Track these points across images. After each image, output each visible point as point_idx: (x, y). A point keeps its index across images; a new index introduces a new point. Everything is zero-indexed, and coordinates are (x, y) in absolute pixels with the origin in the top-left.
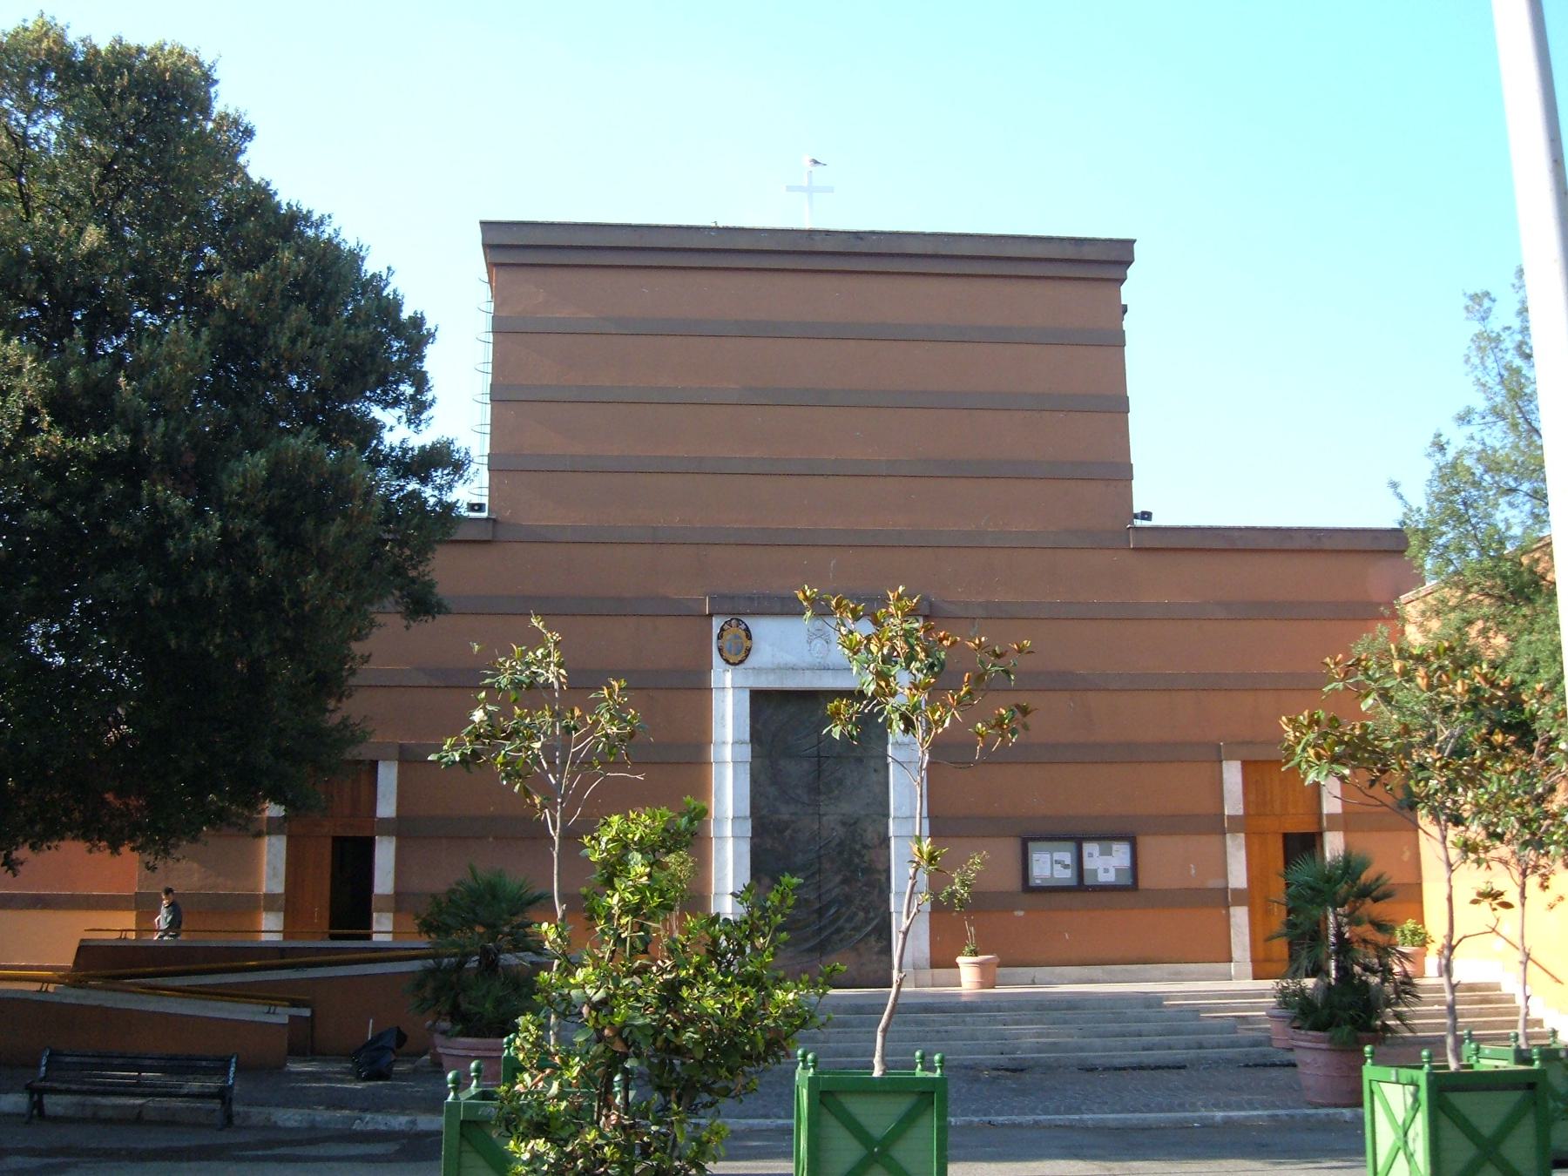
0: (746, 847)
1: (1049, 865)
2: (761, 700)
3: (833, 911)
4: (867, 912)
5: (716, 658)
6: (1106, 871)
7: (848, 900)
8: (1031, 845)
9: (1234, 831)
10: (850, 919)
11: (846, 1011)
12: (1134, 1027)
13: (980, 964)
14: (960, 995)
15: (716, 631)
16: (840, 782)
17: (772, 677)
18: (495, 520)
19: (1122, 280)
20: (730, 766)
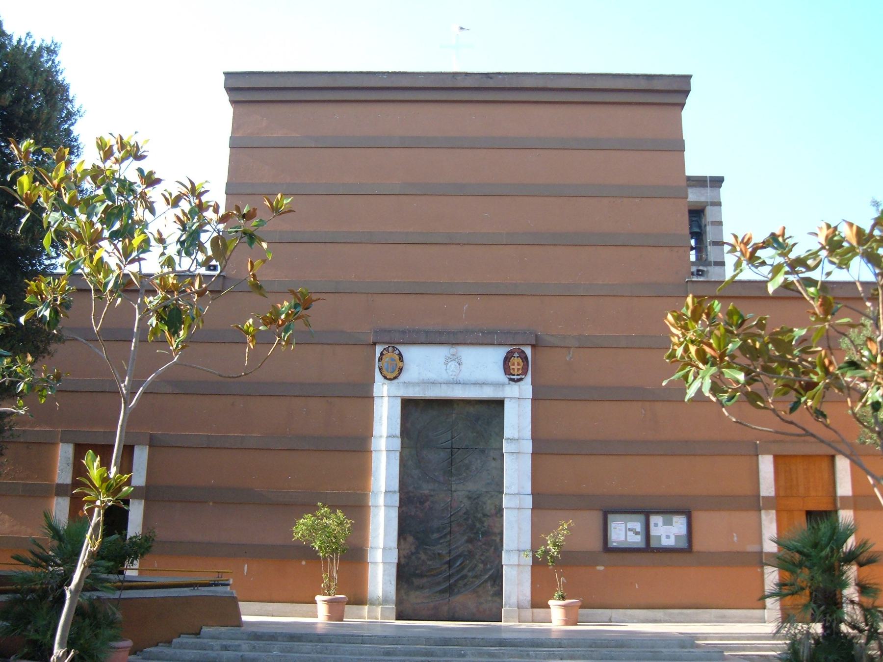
0: (394, 514)
1: (624, 532)
2: (409, 405)
4: (485, 565)
5: (378, 376)
7: (471, 555)
9: (767, 508)
13: (565, 606)
14: (548, 631)
15: (378, 355)
16: (468, 467)
17: (417, 389)
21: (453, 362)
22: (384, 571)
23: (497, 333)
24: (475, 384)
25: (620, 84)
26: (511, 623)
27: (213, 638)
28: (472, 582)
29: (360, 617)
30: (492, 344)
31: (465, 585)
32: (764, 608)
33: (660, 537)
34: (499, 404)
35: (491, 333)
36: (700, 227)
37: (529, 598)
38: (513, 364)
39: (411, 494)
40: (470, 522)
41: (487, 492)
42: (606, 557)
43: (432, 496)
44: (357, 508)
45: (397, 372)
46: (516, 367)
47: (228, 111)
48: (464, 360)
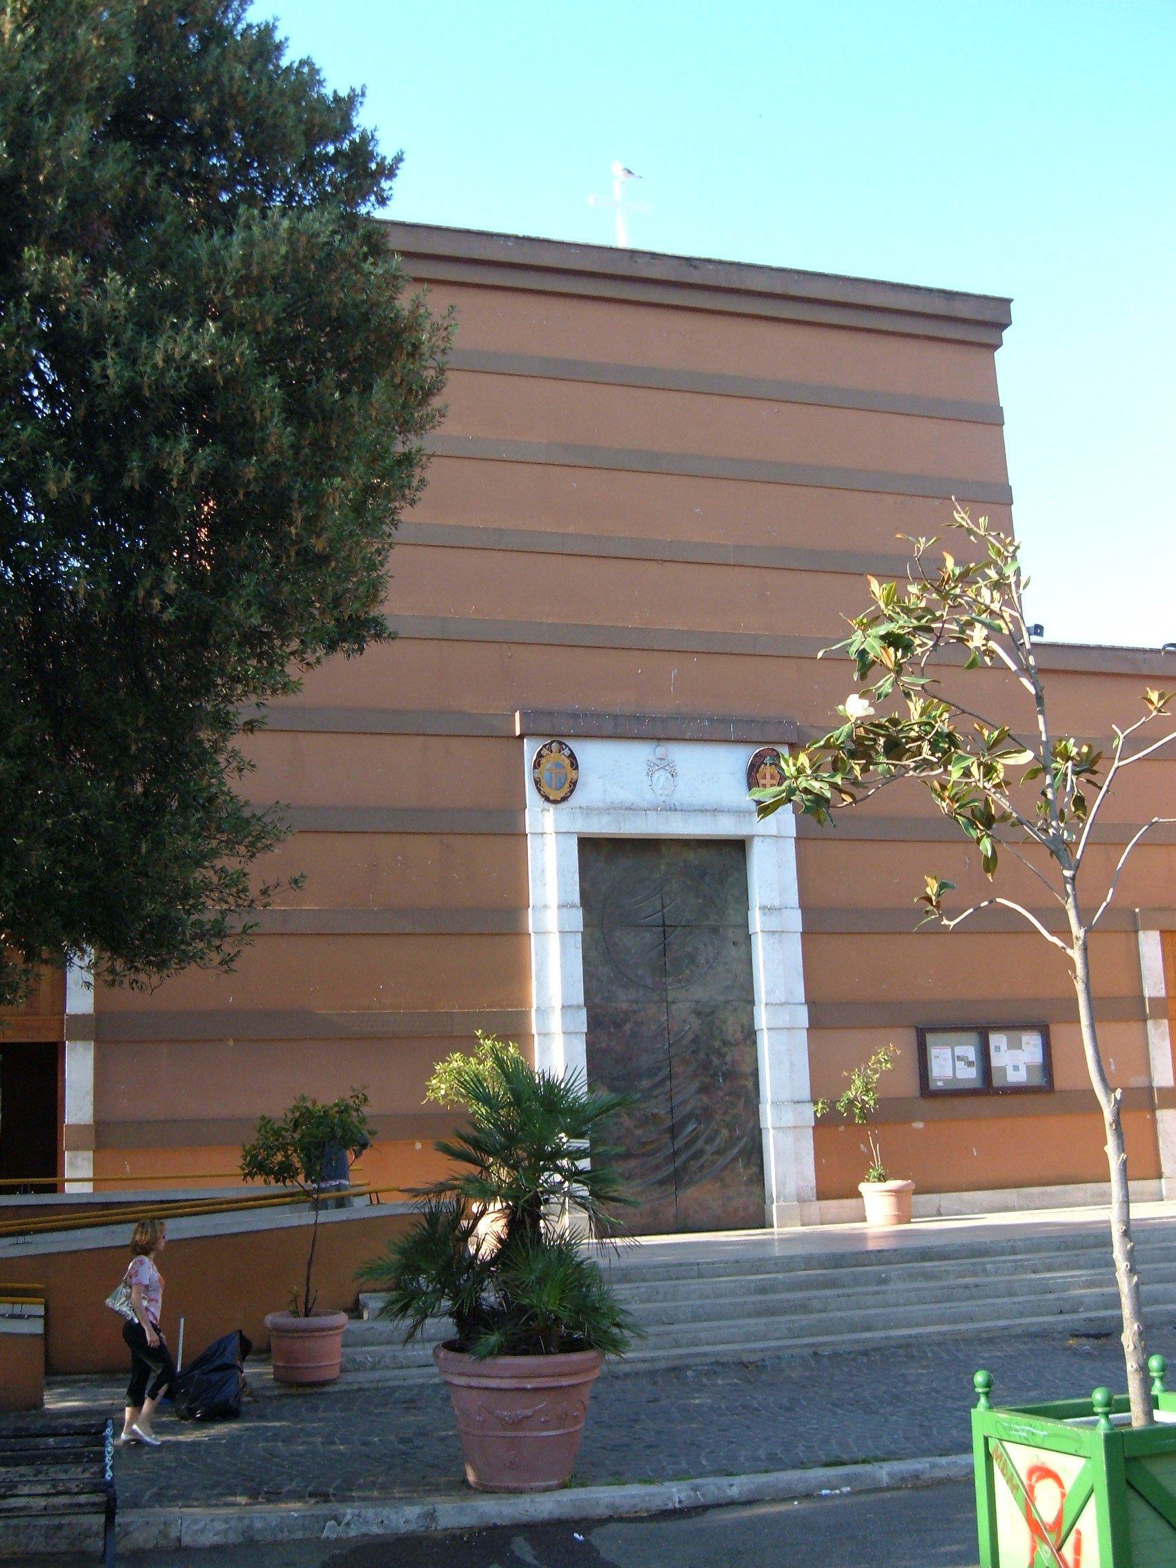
1: (951, 1062)
2: (589, 846)
3: (690, 1127)
4: (732, 1131)
6: (1016, 1068)
8: (930, 1037)
9: (1156, 1016)
10: (710, 1140)
11: (822, 1266)
13: (897, 1193)
14: (862, 1237)
16: (692, 959)
17: (606, 819)
19: (996, 346)
21: (662, 772)
24: (702, 811)
25: (873, 299)
28: (713, 1163)
30: (727, 741)
31: (702, 1167)
32: (1160, 1176)
33: (1004, 1069)
34: (738, 848)
35: (725, 720)
37: (813, 1183)
39: (598, 1011)
40: (702, 1055)
42: (927, 1105)
43: (635, 1012)
45: (566, 789)
48: (678, 770)
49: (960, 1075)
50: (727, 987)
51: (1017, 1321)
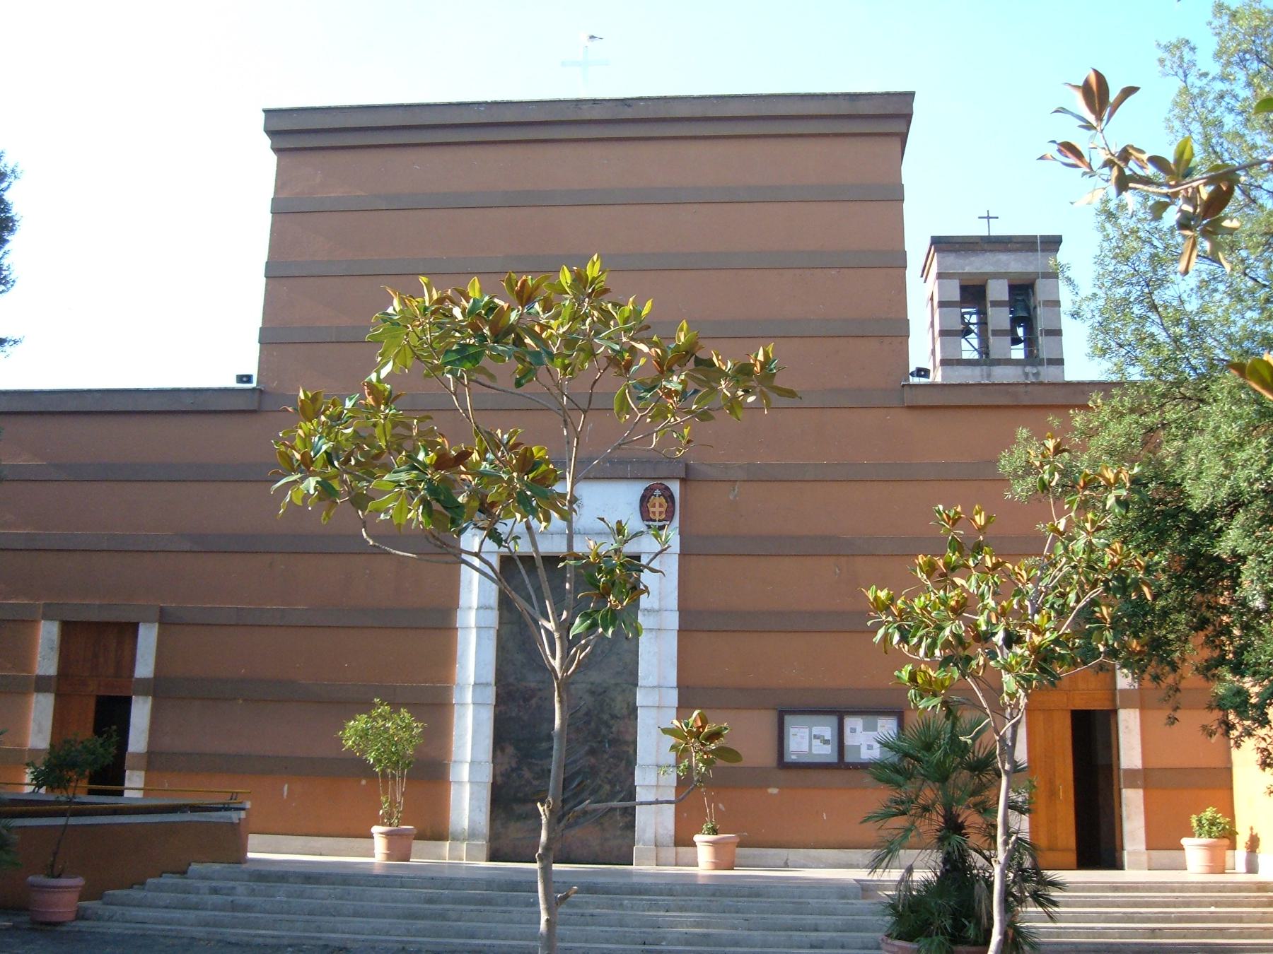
0: (488, 715)
1: (808, 739)
4: (613, 786)
6: (870, 747)
7: (594, 772)
8: (788, 719)
11: (500, 888)
12: (810, 920)
13: (714, 843)
14: (695, 876)
18: (260, 390)
20: (474, 631)
22: (472, 794)
23: (631, 462)
26: (643, 867)
27: (204, 878)
29: (429, 857)
33: (858, 747)
36: (1027, 309)
37: (672, 832)
38: (654, 506)
40: (593, 725)
41: (617, 684)
42: (783, 775)
44: (434, 708)
46: (657, 509)
47: (273, 158)
49: (814, 751)
50: (618, 673)
51: (583, 945)
